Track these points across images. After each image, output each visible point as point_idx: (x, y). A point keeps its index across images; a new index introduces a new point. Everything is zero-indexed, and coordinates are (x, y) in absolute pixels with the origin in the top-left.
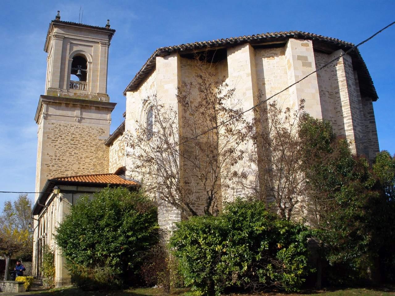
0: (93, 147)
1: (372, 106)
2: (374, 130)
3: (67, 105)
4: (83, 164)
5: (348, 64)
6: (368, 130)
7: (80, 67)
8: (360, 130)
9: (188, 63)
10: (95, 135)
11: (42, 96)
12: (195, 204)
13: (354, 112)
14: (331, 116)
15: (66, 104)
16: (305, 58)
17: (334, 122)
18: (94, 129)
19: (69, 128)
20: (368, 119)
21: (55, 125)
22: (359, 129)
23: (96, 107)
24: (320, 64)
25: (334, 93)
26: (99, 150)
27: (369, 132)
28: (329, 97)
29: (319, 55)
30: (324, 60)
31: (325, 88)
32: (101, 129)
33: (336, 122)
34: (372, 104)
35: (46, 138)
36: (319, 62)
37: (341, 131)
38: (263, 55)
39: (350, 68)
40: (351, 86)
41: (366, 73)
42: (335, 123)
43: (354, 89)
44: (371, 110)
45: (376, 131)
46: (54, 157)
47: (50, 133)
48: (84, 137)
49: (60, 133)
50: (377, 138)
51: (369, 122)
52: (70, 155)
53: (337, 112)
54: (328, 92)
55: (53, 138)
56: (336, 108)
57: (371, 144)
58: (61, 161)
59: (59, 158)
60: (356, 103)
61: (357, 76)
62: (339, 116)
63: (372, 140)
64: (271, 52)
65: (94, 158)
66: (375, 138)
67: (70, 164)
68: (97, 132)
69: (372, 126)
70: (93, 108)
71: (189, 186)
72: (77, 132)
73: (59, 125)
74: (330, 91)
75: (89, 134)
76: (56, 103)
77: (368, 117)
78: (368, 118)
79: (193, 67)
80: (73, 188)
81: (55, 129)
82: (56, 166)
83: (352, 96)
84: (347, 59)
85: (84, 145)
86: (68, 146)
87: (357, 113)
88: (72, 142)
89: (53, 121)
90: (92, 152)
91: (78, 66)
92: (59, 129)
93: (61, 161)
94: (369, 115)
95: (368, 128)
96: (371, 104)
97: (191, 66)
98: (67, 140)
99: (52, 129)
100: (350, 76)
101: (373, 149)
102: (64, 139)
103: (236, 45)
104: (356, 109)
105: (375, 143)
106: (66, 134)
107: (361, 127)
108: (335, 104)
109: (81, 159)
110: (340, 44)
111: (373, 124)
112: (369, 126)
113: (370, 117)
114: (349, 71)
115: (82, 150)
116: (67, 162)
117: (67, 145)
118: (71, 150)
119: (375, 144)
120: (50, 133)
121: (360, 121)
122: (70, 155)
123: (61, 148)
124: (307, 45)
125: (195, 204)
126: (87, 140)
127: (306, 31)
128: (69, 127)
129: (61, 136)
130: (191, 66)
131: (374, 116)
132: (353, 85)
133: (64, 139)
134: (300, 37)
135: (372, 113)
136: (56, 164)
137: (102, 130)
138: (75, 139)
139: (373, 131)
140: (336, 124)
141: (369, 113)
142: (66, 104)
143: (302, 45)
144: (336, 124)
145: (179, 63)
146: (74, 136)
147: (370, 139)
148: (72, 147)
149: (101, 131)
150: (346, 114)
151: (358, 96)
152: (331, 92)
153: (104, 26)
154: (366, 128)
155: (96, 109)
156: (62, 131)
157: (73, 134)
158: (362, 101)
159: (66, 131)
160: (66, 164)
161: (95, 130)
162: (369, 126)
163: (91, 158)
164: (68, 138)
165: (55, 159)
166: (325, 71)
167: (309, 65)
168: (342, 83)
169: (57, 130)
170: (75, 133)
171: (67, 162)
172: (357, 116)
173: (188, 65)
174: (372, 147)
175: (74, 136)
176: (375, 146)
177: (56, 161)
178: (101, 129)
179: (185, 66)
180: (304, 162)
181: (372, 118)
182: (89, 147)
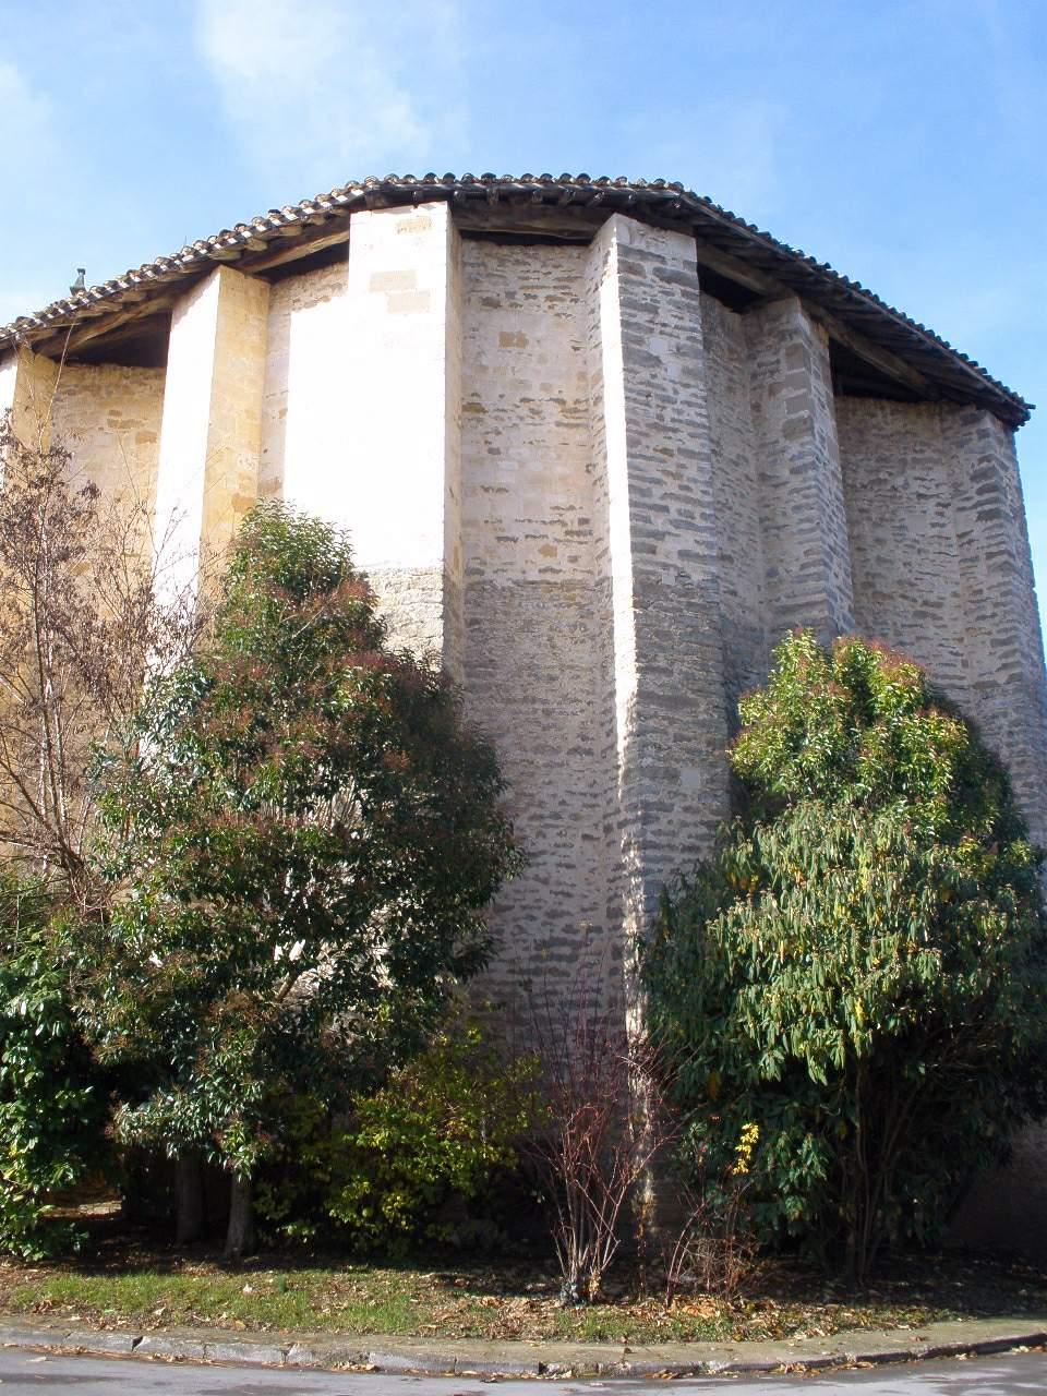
14: (561, 500)
17: (576, 527)
20: (968, 504)
27: (976, 559)
29: (535, 257)
30: (557, 273)
31: (546, 387)
41: (892, 323)
42: (578, 533)
51: (974, 515)
54: (562, 402)
57: (983, 612)
62: (598, 500)
63: (986, 593)
64: (324, 282)
77: (972, 493)
78: (968, 499)
79: (103, 393)
94: (977, 486)
95: (970, 542)
97: (99, 388)
101: (990, 633)
103: (182, 282)
105: (996, 605)
110: (597, 192)
112: (974, 535)
113: (980, 492)
127: (414, 167)
134: (393, 196)
147: (981, 591)
152: (577, 402)
162: (974, 535)
173: (86, 388)
174: (986, 625)
176: (997, 619)
179: (71, 393)
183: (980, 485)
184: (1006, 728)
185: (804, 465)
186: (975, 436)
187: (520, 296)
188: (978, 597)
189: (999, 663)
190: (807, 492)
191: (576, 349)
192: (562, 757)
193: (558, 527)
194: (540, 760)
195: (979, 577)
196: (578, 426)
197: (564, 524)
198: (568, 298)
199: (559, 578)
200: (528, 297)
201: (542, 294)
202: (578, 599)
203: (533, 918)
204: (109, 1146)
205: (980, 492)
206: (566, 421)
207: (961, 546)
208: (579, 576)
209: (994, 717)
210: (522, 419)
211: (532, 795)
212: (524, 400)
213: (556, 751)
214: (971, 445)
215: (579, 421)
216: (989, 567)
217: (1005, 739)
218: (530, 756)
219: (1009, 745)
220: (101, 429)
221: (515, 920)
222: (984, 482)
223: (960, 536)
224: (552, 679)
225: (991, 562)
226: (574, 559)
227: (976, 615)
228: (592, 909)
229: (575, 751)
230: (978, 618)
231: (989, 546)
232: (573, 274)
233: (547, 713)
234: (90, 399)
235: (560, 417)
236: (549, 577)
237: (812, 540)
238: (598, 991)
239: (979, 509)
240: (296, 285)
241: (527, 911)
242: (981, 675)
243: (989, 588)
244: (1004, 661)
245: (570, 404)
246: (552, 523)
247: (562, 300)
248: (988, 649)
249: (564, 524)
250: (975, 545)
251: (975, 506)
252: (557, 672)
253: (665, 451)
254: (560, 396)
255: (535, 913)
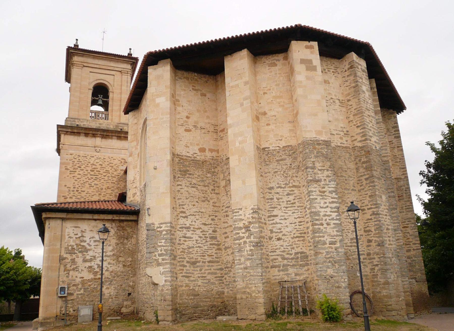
0: (115, 177)
1: (397, 120)
2: (399, 146)
3: (86, 135)
4: (104, 195)
5: (361, 69)
6: (393, 146)
7: (100, 96)
8: (377, 141)
9: (185, 76)
10: (117, 166)
11: (58, 126)
12: (190, 228)
13: (369, 120)
14: (342, 125)
15: (85, 133)
16: (310, 61)
17: (346, 133)
18: (115, 159)
19: (89, 159)
20: (392, 134)
21: (73, 156)
22: (376, 140)
23: (117, 136)
24: (329, 70)
25: (346, 101)
26: (121, 180)
28: (339, 106)
30: (334, 65)
32: (122, 159)
33: (348, 133)
34: (396, 117)
35: (64, 169)
36: (328, 67)
37: (354, 142)
38: (264, 62)
39: (364, 73)
40: (366, 92)
42: (347, 134)
43: (369, 96)
44: (396, 125)
45: (402, 146)
46: (72, 189)
47: (68, 164)
48: (105, 168)
49: (79, 164)
50: (403, 154)
51: (393, 137)
52: (90, 187)
53: (349, 122)
54: (339, 100)
55: (72, 170)
56: (349, 118)
57: (397, 161)
58: (80, 193)
59: (78, 189)
60: (371, 110)
61: (374, 85)
63: (397, 156)
64: (273, 58)
65: (115, 189)
66: (401, 154)
67: (89, 196)
68: (120, 162)
69: (397, 141)
70: (114, 137)
71: (183, 208)
72: (97, 163)
73: (78, 156)
74: (341, 99)
75: (111, 165)
76: (74, 132)
78: (391, 133)
80: (63, 215)
81: (74, 160)
82: (74, 197)
83: (366, 103)
84: (360, 63)
85: (105, 176)
86: (88, 177)
87: (373, 122)
88: (92, 173)
89: (71, 152)
90: (114, 183)
91: (99, 95)
92: (78, 159)
93: (80, 193)
94: (394, 130)
95: (392, 143)
96: (396, 117)
98: (87, 171)
99: (70, 160)
100: (364, 81)
101: (399, 166)
102: (83, 170)
104: (371, 118)
105: (400, 159)
106: (86, 165)
107: (378, 138)
108: (347, 112)
109: (101, 190)
111: (398, 139)
112: (393, 142)
113: (395, 131)
114: (362, 75)
115: (102, 181)
116: (87, 194)
117: (86, 177)
118: (91, 181)
119: (401, 160)
120: (68, 164)
121: (376, 131)
122: (90, 187)
123: (80, 180)
124: (312, 47)
125: (190, 228)
126: (108, 171)
128: (88, 157)
129: (80, 167)
130: (188, 79)
131: (398, 131)
132: (367, 91)
133: (83, 170)
135: (396, 128)
136: (74, 196)
137: (125, 160)
138: (95, 170)
139: (398, 147)
140: (349, 135)
141: (393, 128)
142: (85, 133)
143: (307, 47)
144: (349, 135)
145: (173, 75)
146: (94, 167)
147: (396, 156)
148: (92, 178)
149: (123, 161)
150: (360, 123)
151: (375, 106)
152: (342, 100)
153: (126, 55)
154: (390, 144)
155: (118, 139)
156: (81, 162)
157: (93, 164)
158: (381, 111)
159: (85, 162)
160: (86, 196)
161: (117, 160)
162: (393, 142)
163: (112, 189)
164: (87, 168)
165: (73, 191)
166: (335, 77)
167: (314, 69)
168: (355, 89)
169: (76, 161)
170: (95, 163)
171: (87, 194)
172: (373, 125)
173: (185, 78)
174: (398, 164)
175: (94, 167)
176: (401, 163)
177: (74, 192)
178: (122, 159)
180: (421, 225)
181: (397, 132)
182: (110, 178)
183: (394, 130)
184: (405, 189)
185: (380, 122)
186: (393, 117)
187: (326, 70)
188: (395, 157)
189: (402, 173)
190: (381, 128)
191: (340, 86)
192: (350, 191)
193: (342, 132)
194: (346, 192)
195: (395, 152)
196: (343, 107)
197: (343, 131)
198: (337, 73)
199: (344, 146)
200: (328, 71)
201: (331, 70)
202: (349, 151)
203: (349, 232)
204: (18, 301)
205: (395, 131)
206: (341, 105)
207: (390, 144)
208: (348, 145)
209: (401, 186)
210: (331, 103)
211: (345, 201)
212: (331, 98)
213: (349, 189)
214: (392, 119)
215: (343, 105)
216: (398, 150)
217: (405, 192)
218: (344, 191)
219: (406, 193)
220: (190, 90)
221: (345, 233)
222: (396, 129)
223: (389, 142)
224: (346, 171)
225: (398, 149)
226: (347, 141)
227: (395, 161)
228: (360, 230)
229: (353, 190)
230: (395, 162)
231: (398, 145)
232: (337, 66)
233: (346, 180)
234: (186, 81)
235: (339, 104)
236: (342, 145)
237: (383, 141)
238: (364, 251)
239: (395, 135)
240: (263, 58)
241: (348, 231)
242: (397, 176)
243: (398, 155)
244: (403, 173)
245: (341, 101)
246: (341, 131)
247: (336, 73)
248: (399, 170)
249: (343, 131)
250: (394, 144)
251: (393, 135)
252: (346, 169)
253: (369, 115)
254: (339, 98)
255: (349, 231)
